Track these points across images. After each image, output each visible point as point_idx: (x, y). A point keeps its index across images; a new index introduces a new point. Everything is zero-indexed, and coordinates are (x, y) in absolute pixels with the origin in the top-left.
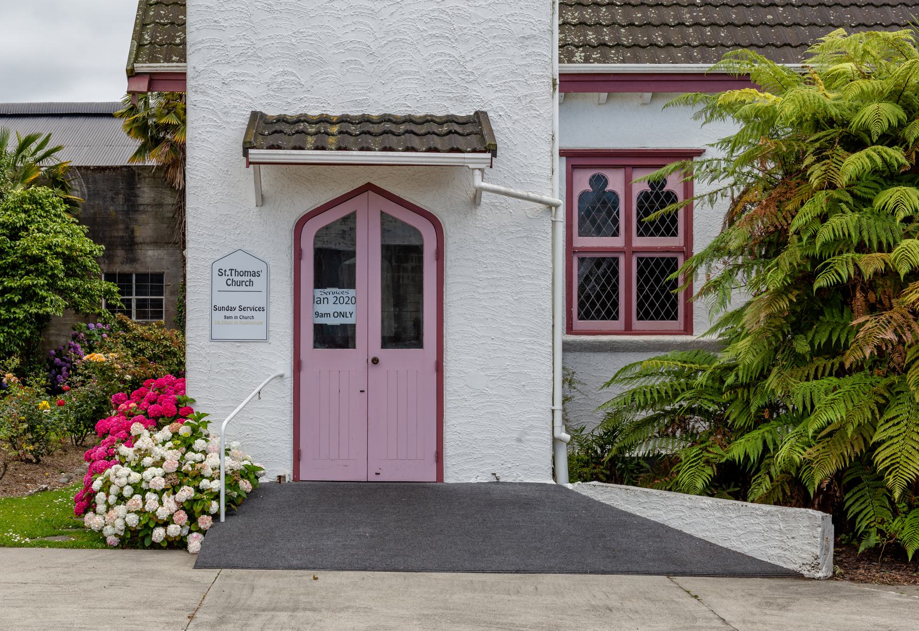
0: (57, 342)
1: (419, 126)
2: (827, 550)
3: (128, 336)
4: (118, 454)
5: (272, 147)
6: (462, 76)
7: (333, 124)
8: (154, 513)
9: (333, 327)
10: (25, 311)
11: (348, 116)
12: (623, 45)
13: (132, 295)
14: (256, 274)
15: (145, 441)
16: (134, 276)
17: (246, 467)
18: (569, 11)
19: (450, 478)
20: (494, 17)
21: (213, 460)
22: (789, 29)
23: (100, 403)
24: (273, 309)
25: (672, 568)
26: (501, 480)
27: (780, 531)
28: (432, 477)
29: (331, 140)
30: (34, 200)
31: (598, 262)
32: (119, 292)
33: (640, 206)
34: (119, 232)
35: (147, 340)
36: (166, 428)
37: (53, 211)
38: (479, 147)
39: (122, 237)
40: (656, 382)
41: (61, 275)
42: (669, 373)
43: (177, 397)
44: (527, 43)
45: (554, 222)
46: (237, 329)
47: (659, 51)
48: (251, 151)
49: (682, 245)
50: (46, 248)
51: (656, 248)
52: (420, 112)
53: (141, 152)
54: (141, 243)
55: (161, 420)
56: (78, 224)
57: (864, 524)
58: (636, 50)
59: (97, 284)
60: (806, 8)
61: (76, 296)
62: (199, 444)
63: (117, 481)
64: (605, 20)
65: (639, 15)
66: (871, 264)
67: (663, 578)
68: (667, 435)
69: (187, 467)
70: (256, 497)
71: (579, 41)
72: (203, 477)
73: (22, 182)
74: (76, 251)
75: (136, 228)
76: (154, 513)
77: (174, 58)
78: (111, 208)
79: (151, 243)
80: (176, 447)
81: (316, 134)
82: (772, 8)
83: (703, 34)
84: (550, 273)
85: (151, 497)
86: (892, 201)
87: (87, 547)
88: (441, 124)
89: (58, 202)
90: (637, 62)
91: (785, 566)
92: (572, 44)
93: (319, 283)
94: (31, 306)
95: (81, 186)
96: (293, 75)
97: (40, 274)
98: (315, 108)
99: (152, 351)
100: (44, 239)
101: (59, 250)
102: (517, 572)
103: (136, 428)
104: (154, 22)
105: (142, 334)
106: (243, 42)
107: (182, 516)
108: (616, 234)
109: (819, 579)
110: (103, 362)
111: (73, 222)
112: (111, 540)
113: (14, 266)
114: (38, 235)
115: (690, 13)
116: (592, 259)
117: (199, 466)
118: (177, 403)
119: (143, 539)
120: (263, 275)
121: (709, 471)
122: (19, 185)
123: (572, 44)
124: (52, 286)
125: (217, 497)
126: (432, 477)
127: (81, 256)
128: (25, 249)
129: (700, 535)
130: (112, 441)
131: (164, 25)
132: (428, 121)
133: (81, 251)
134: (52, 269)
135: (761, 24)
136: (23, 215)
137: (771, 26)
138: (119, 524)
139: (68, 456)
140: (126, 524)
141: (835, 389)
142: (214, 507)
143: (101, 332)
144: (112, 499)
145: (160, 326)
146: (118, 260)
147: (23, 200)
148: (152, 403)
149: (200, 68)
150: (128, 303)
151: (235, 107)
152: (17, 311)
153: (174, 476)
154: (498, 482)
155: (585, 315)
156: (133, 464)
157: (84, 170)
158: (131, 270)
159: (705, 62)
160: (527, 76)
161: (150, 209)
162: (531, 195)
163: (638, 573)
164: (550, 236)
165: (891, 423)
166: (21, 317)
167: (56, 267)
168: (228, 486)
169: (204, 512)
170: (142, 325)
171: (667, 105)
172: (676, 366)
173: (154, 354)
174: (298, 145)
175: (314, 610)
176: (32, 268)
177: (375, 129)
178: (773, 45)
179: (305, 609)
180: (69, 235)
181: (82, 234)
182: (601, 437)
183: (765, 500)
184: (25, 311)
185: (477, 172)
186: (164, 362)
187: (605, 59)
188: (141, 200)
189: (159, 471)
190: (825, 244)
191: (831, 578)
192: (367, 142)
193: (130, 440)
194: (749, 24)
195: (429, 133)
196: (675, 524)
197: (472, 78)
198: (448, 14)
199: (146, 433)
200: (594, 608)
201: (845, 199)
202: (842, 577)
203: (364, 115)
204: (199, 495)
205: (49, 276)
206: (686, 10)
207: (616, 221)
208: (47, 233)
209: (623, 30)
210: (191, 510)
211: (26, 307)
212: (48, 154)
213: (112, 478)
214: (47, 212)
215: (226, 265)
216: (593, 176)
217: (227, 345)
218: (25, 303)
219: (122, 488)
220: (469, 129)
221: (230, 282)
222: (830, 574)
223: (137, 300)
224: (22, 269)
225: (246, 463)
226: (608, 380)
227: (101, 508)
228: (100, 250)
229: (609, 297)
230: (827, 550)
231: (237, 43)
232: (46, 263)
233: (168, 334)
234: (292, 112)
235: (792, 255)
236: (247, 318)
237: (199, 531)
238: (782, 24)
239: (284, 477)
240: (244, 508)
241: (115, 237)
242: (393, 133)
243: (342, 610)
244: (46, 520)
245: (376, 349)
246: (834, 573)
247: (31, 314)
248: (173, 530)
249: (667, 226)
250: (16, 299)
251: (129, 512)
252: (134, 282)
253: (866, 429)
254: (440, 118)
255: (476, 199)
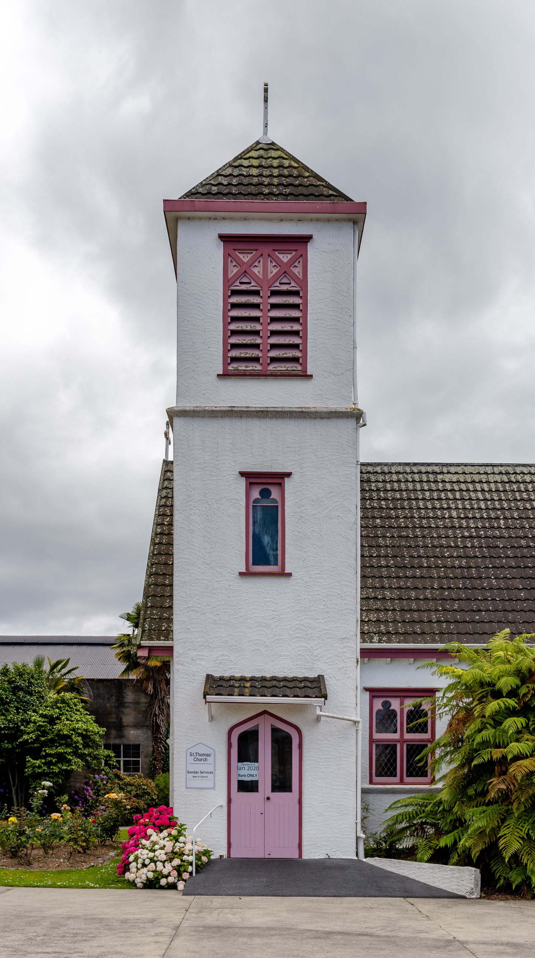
0: (74, 786)
1: (290, 683)
2: (477, 885)
3: (121, 783)
4: (141, 844)
5: (217, 694)
6: (312, 657)
7: (247, 681)
8: (161, 872)
9: (247, 782)
10: (59, 768)
11: (254, 677)
12: (399, 633)
13: (120, 758)
14: (208, 755)
15: (154, 838)
16: (122, 746)
17: (205, 850)
18: (372, 613)
19: (306, 856)
20: (328, 628)
21: (189, 847)
22: (487, 624)
23: (115, 821)
24: (217, 772)
25: (407, 894)
26: (331, 857)
27: (457, 878)
28: (296, 856)
29: (247, 690)
30: (63, 701)
31: (386, 747)
32: (115, 757)
33: (408, 717)
34: (113, 719)
35: (133, 785)
36: (165, 831)
37: (75, 708)
38: (318, 695)
39: (115, 722)
40: (410, 809)
41: (81, 747)
42: (416, 805)
43: (169, 816)
44: (344, 641)
45: (357, 730)
46: (199, 783)
47: (418, 636)
48: (207, 696)
49: (430, 737)
50: (72, 730)
51: (416, 739)
52: (290, 675)
53: (126, 671)
54: (126, 726)
55: (162, 828)
56: (89, 715)
57: (498, 875)
58: (406, 636)
59: (101, 752)
60: (497, 612)
61: (89, 759)
62: (182, 839)
63: (142, 857)
64: (391, 619)
65: (409, 616)
66: (497, 754)
67: (402, 899)
68: (414, 836)
69: (177, 850)
70: (210, 865)
71: (376, 631)
72: (184, 854)
73: (54, 689)
74: (90, 732)
75: (123, 717)
76: (161, 872)
77: (162, 638)
78: (108, 705)
79: (133, 726)
80: (171, 840)
81: (239, 687)
82: (479, 612)
83: (442, 627)
84: (355, 755)
85: (159, 864)
86: (507, 725)
87: (127, 888)
88: (301, 682)
89: (78, 702)
90: (406, 643)
91: (459, 894)
92: (372, 632)
93: (241, 759)
94: (63, 765)
95: (89, 691)
96: (227, 656)
97: (68, 746)
98: (238, 673)
99: (136, 791)
100: (70, 725)
101: (79, 731)
102: (334, 896)
103: (150, 831)
104: (150, 617)
105: (129, 782)
106: (202, 639)
107: (175, 873)
108: (395, 732)
109: (473, 899)
110: (116, 799)
111: (87, 714)
112: (139, 885)
113: (52, 741)
114: (67, 722)
115: (436, 615)
116: (382, 745)
117: (183, 849)
118: (170, 819)
119: (155, 884)
120: (212, 756)
121: (431, 852)
122: (52, 691)
123: (372, 632)
124: (75, 753)
125: (191, 864)
126: (296, 856)
127: (92, 735)
128: (59, 731)
129: (423, 881)
130: (137, 838)
131: (156, 619)
132: (294, 680)
133: (92, 732)
134: (75, 743)
135: (472, 621)
136: (57, 710)
137: (478, 623)
138: (144, 877)
139: (98, 850)
140: (147, 877)
141: (484, 812)
142: (190, 869)
143: (102, 780)
144: (140, 866)
145: (140, 777)
146: (112, 736)
147: (57, 702)
148: (156, 819)
149: (181, 652)
150: (118, 762)
151: (198, 672)
152: (55, 768)
153: (171, 854)
154: (329, 858)
155: (379, 775)
156: (149, 848)
157: (92, 682)
158: (120, 742)
159: (441, 643)
160: (344, 658)
161: (131, 705)
162: (345, 717)
163: (390, 897)
164: (355, 737)
165: (506, 828)
166: (57, 771)
167: (78, 742)
168: (196, 859)
169: (185, 871)
170: (129, 776)
171: (418, 668)
172: (421, 802)
173: (137, 794)
174: (230, 693)
175: (241, 908)
176: (63, 742)
177: (268, 684)
178: (478, 633)
179: (236, 908)
180: (84, 723)
181: (92, 721)
182: (384, 837)
183: (456, 864)
184: (59, 768)
185: (318, 707)
186: (143, 798)
187: (389, 641)
188: (126, 700)
189: (163, 852)
190: (478, 744)
191: (479, 898)
192: (264, 692)
193: (147, 837)
194: (466, 622)
195: (295, 687)
196: (411, 876)
197: (317, 658)
198: (305, 626)
199: (155, 834)
200: (365, 908)
201: (489, 722)
202: (484, 898)
203: (263, 676)
204: (183, 863)
205: (74, 747)
206: (433, 613)
207: (395, 725)
208: (72, 721)
209: (399, 624)
210: (179, 870)
211: (60, 765)
212: (69, 672)
213: (139, 855)
214: (71, 708)
215: (194, 751)
216: (384, 702)
217: (194, 790)
218: (59, 763)
219: (144, 860)
220: (315, 685)
221: (195, 759)
222: (479, 896)
223: (124, 761)
224: (57, 743)
225: (204, 848)
226: (387, 808)
227: (134, 870)
228: (103, 731)
229: (392, 765)
230: (477, 885)
231: (199, 640)
232: (72, 739)
233: (145, 782)
234: (227, 674)
235: (465, 748)
236: (204, 777)
237: (183, 880)
238: (483, 622)
239: (223, 856)
240: (204, 870)
241: (111, 722)
242: (277, 687)
243: (253, 908)
244: (101, 878)
245: (269, 793)
246: (481, 896)
247: (63, 770)
248: (171, 879)
249: (422, 728)
250: (54, 761)
251: (148, 871)
252: (122, 750)
253: (495, 830)
254: (301, 678)
255: (318, 719)
